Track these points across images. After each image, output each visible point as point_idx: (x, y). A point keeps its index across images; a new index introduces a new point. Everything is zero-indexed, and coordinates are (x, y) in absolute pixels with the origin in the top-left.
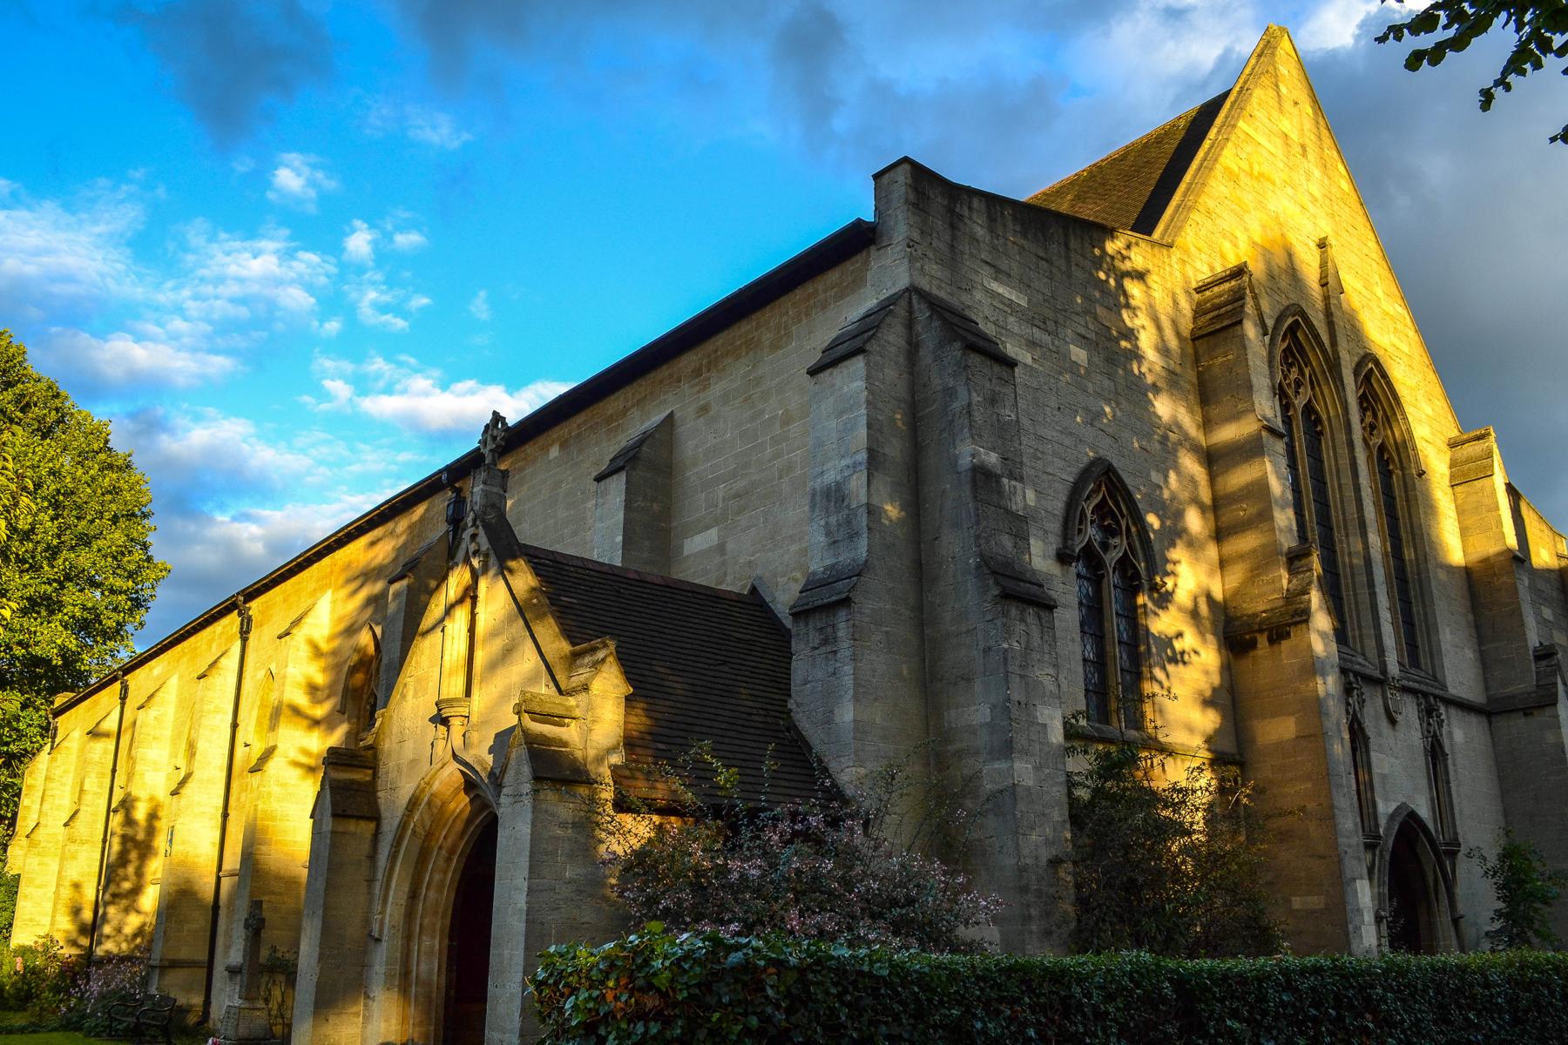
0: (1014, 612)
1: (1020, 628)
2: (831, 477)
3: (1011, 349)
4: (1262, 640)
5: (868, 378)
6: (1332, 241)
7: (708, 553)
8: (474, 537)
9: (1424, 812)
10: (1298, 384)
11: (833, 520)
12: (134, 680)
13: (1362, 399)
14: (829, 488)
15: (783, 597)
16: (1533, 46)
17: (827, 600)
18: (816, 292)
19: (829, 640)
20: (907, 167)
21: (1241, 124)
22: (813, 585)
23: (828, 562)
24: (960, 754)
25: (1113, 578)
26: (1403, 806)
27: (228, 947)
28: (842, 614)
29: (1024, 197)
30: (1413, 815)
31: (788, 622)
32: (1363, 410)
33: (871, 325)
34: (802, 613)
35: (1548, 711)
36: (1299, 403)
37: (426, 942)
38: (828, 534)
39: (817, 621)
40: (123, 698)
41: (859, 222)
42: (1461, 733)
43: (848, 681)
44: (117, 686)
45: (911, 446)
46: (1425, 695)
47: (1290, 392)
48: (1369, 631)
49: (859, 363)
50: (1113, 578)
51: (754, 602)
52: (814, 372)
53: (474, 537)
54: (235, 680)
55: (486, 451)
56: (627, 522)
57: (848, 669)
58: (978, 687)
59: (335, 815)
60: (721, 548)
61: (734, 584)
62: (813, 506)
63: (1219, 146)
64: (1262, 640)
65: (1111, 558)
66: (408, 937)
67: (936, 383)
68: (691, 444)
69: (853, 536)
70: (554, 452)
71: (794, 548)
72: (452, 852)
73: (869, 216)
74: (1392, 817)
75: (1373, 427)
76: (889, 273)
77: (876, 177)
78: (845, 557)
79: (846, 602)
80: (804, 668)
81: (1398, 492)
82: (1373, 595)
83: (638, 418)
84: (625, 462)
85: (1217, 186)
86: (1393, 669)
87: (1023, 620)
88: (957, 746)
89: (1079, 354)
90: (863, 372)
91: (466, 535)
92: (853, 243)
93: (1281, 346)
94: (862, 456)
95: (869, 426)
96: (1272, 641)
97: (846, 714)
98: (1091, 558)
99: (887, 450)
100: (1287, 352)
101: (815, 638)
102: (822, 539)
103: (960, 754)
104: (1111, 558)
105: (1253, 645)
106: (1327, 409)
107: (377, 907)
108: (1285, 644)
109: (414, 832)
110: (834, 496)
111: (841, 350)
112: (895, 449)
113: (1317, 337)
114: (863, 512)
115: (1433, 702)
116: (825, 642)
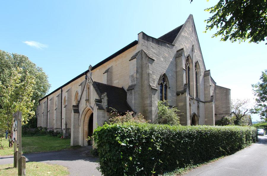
0: (153, 90)
1: (153, 92)
2: (132, 74)
3: (154, 59)
4: (181, 94)
5: (137, 61)
6: (194, 45)
7: (117, 83)
8: (88, 80)
9: (196, 113)
10: (188, 64)
11: (132, 79)
12: (49, 97)
13: (195, 66)
14: (131, 75)
15: (126, 88)
16: (242, 6)
17: (131, 88)
18: (130, 50)
19: (131, 93)
20: (142, 33)
21: (185, 29)
22: (129, 87)
23: (131, 84)
24: (146, 106)
25: (164, 87)
26: (194, 113)
27: (63, 126)
28: (133, 90)
29: (157, 38)
30: (195, 113)
31: (126, 91)
32: (195, 67)
33: (137, 54)
34: (128, 90)
35: (212, 103)
36: (187, 66)
37: (86, 126)
38: (131, 81)
39: (130, 91)
40: (48, 99)
41: (136, 40)
42: (201, 105)
43: (134, 98)
44: (47, 98)
45: (141, 70)
46: (198, 100)
47: (187, 65)
48: (192, 92)
49: (135, 59)
50: (164, 87)
51: (122, 89)
52: (130, 60)
53: (88, 80)
54: (56, 92)
55: (89, 70)
56: (107, 79)
57: (134, 97)
58: (148, 99)
59: (74, 113)
60: (119, 83)
61: (120, 86)
62: (130, 77)
63: (181, 32)
64: (181, 94)
65: (164, 84)
66: (84, 126)
67: (145, 62)
68: (96, 94)
69: (134, 81)
70: (98, 70)
71: (127, 82)
72: (88, 116)
73: (137, 40)
74: (193, 114)
75: (196, 69)
76: (137, 48)
77: (138, 34)
78: (133, 83)
79: (134, 89)
80: (128, 96)
81: (198, 77)
82: (193, 89)
83: (107, 65)
84: (107, 71)
85: (180, 39)
86: (195, 98)
87: (154, 91)
88: (146, 105)
89: (162, 59)
90: (136, 61)
91: (88, 80)
92: (135, 43)
93: (186, 59)
94: (136, 71)
95: (137, 68)
96: (182, 94)
97: (133, 102)
98: (162, 85)
99: (139, 71)
100: (187, 60)
101: (130, 93)
102: (131, 82)
103: (146, 106)
104: (164, 84)
105: (179, 94)
106: (191, 67)
107: (80, 123)
108: (183, 95)
109: (43, 122)
110: (132, 76)
111: (133, 58)
112: (140, 71)
113: (191, 58)
114: (136, 78)
115: (198, 101)
116: (131, 94)
